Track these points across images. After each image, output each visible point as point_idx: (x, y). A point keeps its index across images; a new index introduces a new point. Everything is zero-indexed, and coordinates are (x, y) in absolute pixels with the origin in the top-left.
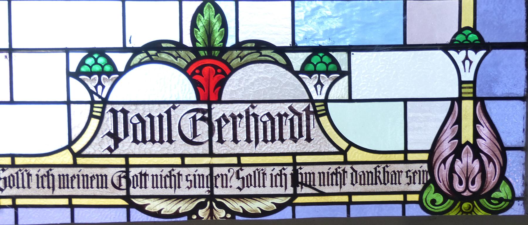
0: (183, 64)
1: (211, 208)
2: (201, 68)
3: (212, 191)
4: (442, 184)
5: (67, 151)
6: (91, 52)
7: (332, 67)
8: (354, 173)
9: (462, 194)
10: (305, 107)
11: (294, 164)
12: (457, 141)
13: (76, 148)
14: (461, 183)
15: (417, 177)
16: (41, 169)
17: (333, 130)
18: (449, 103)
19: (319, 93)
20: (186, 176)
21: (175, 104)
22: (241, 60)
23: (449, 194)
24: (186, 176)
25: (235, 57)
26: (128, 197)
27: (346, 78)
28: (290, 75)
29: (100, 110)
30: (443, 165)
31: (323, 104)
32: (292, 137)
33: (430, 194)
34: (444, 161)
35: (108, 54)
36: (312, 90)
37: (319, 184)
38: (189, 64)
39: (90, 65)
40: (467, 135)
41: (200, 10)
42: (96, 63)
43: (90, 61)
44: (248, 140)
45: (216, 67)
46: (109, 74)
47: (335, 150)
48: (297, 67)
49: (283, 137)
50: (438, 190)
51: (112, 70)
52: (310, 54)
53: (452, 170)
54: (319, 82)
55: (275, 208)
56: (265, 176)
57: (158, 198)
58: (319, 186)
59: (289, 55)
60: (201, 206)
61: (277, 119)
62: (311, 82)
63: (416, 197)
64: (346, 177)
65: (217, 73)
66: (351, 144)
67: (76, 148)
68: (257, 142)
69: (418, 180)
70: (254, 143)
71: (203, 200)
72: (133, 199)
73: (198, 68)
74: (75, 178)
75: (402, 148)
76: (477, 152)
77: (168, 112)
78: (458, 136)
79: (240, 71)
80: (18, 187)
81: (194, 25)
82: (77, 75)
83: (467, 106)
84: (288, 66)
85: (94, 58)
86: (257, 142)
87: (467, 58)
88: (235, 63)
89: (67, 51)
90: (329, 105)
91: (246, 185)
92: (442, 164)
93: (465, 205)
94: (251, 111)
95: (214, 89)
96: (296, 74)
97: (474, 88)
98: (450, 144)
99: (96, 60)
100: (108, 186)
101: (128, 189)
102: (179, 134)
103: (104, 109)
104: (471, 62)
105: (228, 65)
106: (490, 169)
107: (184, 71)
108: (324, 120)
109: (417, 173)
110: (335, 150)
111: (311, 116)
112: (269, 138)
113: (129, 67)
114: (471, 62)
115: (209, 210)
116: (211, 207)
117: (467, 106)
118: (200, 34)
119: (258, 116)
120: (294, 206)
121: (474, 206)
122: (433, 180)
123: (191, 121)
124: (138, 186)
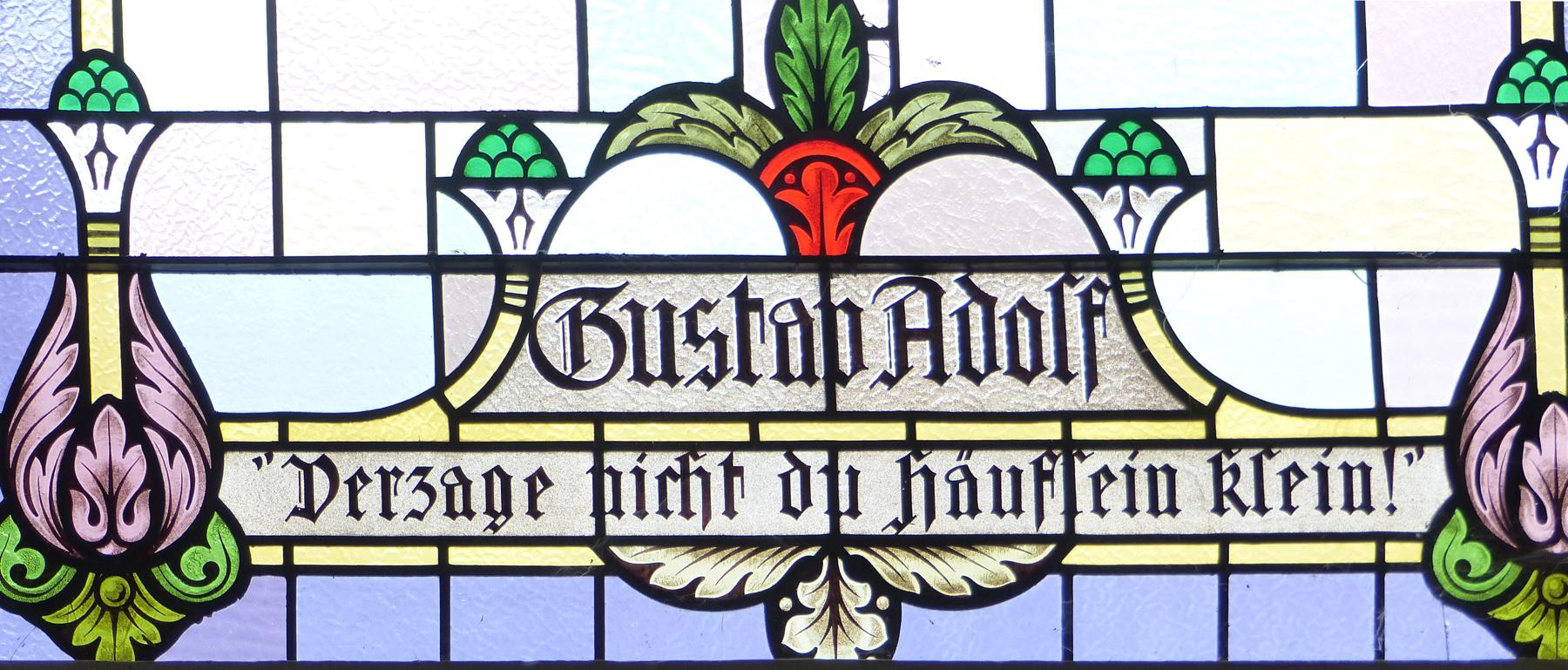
0: (749, 155)
1: (834, 576)
2: (798, 167)
3: (835, 524)
4: (1490, 514)
6: (492, 121)
9: (98, 550)
12: (77, 390)
13: (458, 395)
16: (647, 453)
17: (484, 355)
18: (1493, 276)
20: (781, 476)
23: (64, 548)
24: (781, 476)
26: (600, 541)
27: (1201, 198)
28: (1045, 185)
29: (524, 290)
32: (967, 370)
33: (1455, 546)
34: (41, 452)
35: (539, 125)
37: (1281, 503)
38: (766, 158)
40: (106, 379)
45: (842, 167)
48: (1064, 165)
50: (1477, 531)
53: (67, 479)
55: (1012, 579)
56: (737, 480)
57: (689, 546)
59: (1038, 125)
60: (805, 571)
62: (1105, 209)
66: (1224, 390)
67: (458, 395)
69: (634, 500)
70: (1082, 378)
71: (812, 552)
72: (613, 549)
75: (1370, 403)
76: (136, 422)
78: (80, 375)
81: (775, 42)
82: (454, 185)
83: (104, 288)
84: (1042, 164)
85: (503, 136)
87: (100, 145)
88: (890, 158)
89: (430, 119)
92: (36, 459)
93: (110, 586)
96: (1065, 185)
97: (124, 235)
102: (533, 359)
104: (112, 159)
105: (874, 159)
106: (176, 475)
107: (752, 174)
108: (1145, 322)
110: (1177, 405)
113: (600, 163)
114: (112, 159)
115: (828, 583)
117: (104, 288)
118: (794, 67)
119: (674, 308)
120: (1069, 573)
121: (134, 588)
123: (888, 314)
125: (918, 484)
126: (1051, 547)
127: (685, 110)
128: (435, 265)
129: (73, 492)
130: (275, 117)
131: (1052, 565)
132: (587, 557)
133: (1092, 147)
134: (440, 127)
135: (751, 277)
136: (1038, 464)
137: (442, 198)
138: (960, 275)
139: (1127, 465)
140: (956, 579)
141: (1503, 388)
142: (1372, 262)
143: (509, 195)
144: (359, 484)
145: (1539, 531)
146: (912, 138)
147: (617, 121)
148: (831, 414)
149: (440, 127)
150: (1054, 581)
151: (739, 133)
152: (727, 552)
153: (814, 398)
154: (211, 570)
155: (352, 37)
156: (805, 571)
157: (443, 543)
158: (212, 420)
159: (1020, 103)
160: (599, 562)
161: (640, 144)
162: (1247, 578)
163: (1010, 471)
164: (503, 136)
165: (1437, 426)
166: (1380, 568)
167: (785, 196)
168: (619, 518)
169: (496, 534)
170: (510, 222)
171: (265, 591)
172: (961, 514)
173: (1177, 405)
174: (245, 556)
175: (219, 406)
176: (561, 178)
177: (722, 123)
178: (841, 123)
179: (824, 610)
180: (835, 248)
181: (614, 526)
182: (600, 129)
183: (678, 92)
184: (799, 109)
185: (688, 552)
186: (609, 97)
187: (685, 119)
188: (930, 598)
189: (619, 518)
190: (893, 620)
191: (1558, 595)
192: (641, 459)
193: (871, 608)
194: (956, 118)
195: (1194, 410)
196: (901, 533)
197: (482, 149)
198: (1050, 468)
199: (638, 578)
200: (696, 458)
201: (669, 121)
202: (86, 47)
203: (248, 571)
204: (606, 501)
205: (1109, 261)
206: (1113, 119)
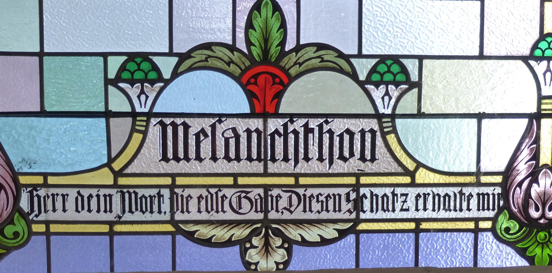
1: (267, 236)
2: (256, 76)
5: (106, 169)
6: (132, 56)
8: (80, 198)
10: (304, 123)
11: (172, 187)
13: (117, 166)
14: (537, 209)
15: (331, 202)
18: (526, 121)
21: (221, 117)
25: (292, 64)
26: (172, 222)
27: (416, 90)
30: (518, 189)
31: (389, 120)
33: (504, 222)
34: (520, 185)
36: (379, 102)
38: (243, 72)
39: (132, 71)
41: (257, 7)
44: (321, 159)
45: (274, 76)
46: (152, 82)
47: (400, 170)
50: (512, 216)
52: (401, 60)
54: (387, 93)
56: (396, 197)
59: (353, 60)
60: (255, 233)
62: (377, 93)
63: (488, 225)
64: (463, 201)
65: (274, 83)
66: (419, 165)
67: (117, 166)
68: (296, 162)
70: (327, 161)
73: (252, 77)
74: (331, 198)
77: (213, 127)
80: (217, 212)
81: (249, 25)
82: (114, 82)
84: (354, 76)
85: (136, 62)
86: (296, 162)
88: (293, 72)
89: (105, 55)
90: (398, 121)
91: (127, 209)
95: (272, 101)
96: (362, 84)
98: (526, 166)
100: (225, 209)
101: (173, 213)
103: (148, 122)
105: (286, 71)
108: (391, 138)
109: (331, 198)
110: (400, 170)
111: (385, 131)
113: (176, 74)
115: (264, 238)
118: (255, 37)
120: (358, 233)
122: (507, 207)
124: (214, 210)
125: (36, 199)
126: (352, 224)
130: (41, 55)
131: (352, 230)
132: (169, 228)
133: (373, 70)
134: (110, 58)
135: (310, 119)
137: (110, 87)
138: (325, 119)
141: (526, 164)
142: (43, 113)
143: (382, 88)
144: (189, 199)
146: (300, 65)
148: (266, 174)
149: (110, 58)
150: (351, 238)
151: (233, 62)
152: (225, 225)
153: (258, 167)
154: (16, 234)
155: (473, 23)
156: (255, 233)
158: (15, 175)
159: (346, 52)
160: (173, 229)
161: (193, 67)
164: (386, 64)
166: (476, 231)
170: (383, 98)
171: (38, 243)
172: (219, 212)
173: (128, 171)
174: (30, 229)
176: (160, 78)
177: (226, 59)
179: (263, 247)
181: (179, 216)
182: (175, 60)
183: (208, 46)
184: (256, 51)
186: (181, 48)
187: (210, 56)
188: (304, 242)
190: (289, 251)
191: (542, 239)
192: (305, 191)
193: (281, 247)
195: (407, 172)
196: (121, 220)
199: (190, 236)
200: (37, 191)
201: (204, 57)
203: (31, 233)
205: (134, 114)
206: (383, 59)
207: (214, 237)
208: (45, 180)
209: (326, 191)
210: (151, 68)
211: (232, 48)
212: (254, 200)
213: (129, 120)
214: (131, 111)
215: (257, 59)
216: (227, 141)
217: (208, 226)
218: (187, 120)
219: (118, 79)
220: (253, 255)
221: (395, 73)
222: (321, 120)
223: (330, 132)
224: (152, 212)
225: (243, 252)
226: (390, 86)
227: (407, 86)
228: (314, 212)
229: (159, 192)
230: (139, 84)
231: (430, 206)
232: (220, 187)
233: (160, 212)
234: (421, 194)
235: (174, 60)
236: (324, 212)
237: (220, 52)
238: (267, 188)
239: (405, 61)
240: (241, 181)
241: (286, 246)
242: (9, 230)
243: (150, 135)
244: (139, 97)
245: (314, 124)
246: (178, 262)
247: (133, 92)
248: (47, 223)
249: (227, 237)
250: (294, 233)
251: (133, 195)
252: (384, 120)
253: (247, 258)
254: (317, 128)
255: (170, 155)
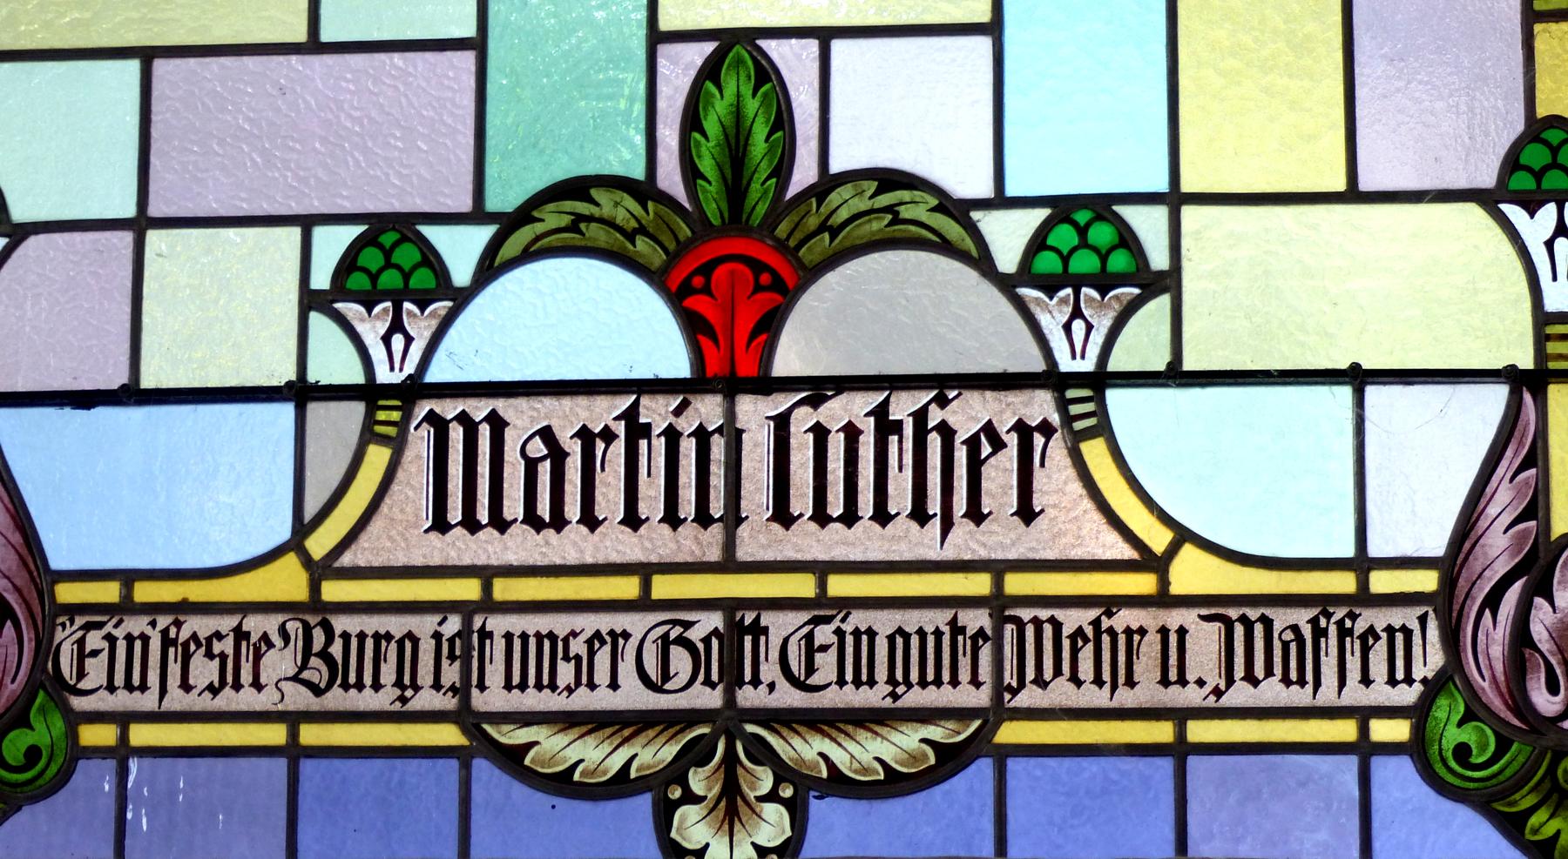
2: (707, 270)
7: (1120, 262)
13: (319, 544)
18: (1498, 395)
19: (397, 366)
22: (832, 240)
26: (466, 717)
27: (1164, 301)
34: (1493, 601)
36: (378, 353)
38: (673, 258)
42: (1084, 244)
43: (1064, 236)
45: (757, 266)
48: (1007, 259)
49: (708, 508)
51: (1133, 269)
56: (488, 642)
58: (874, 688)
60: (695, 754)
61: (575, 448)
64: (1323, 653)
66: (1183, 535)
67: (319, 544)
71: (704, 730)
74: (603, 642)
75: (1348, 550)
79: (831, 279)
81: (692, 121)
84: (982, 261)
85: (1075, 224)
89: (307, 223)
90: (1116, 398)
91: (1239, 671)
94: (935, 416)
95: (751, 339)
96: (1007, 284)
99: (1082, 231)
108: (1094, 451)
112: (836, 508)
116: (730, 760)
127: (583, 208)
128: (301, 393)
129: (1527, 652)
133: (1038, 243)
136: (1314, 622)
139: (436, 631)
140: (866, 758)
144: (264, 648)
145: (1545, 702)
146: (834, 232)
147: (510, 223)
148: (729, 564)
150: (982, 769)
153: (709, 544)
154: (33, 753)
156: (695, 754)
157: (294, 719)
162: (324, 763)
163: (125, 638)
165: (1427, 581)
167: (696, 303)
168: (1367, 687)
169: (405, 708)
170: (1067, 328)
171: (95, 780)
173: (1127, 552)
174: (73, 735)
175: (57, 562)
176: (443, 285)
178: (757, 219)
180: (746, 369)
183: (577, 188)
184: (713, 205)
185: (558, 732)
186: (504, 196)
188: (838, 784)
189: (1367, 687)
190: (797, 812)
193: (772, 797)
194: (889, 209)
197: (1050, 241)
198: (1350, 626)
199: (512, 759)
201: (565, 220)
202: (1541, 112)
203: (78, 753)
204: (717, 670)
206: (1062, 207)
207: (580, 768)
208: (487, 588)
209: (589, 623)
210: (1116, 240)
211: (644, 190)
212: (701, 646)
213: (357, 409)
214: (364, 382)
215: (716, 221)
216: (531, 465)
217: (519, 728)
218: (502, 406)
219: (340, 288)
220: (692, 827)
221: (407, 268)
222: (926, 396)
223: (946, 431)
224: (237, 686)
225: (664, 815)
226: (1085, 290)
227: (449, 304)
228: (195, 692)
229: (954, 620)
230: (388, 304)
231: (1378, 669)
232: (1110, 604)
233: (257, 685)
234: (604, 633)
235: (482, 235)
236: (583, 690)
237: (607, 203)
238: (729, 606)
239: (1128, 212)
240: (664, 587)
241: (787, 792)
242: (16, 744)
243: (409, 455)
244: (1067, 328)
245: (903, 407)
246: (1354, 852)
247: (372, 330)
248: (122, 720)
249: (616, 762)
250: (807, 749)
251: (1259, 629)
252: (1071, 394)
253: (673, 834)
254: (911, 419)
255: (455, 514)
